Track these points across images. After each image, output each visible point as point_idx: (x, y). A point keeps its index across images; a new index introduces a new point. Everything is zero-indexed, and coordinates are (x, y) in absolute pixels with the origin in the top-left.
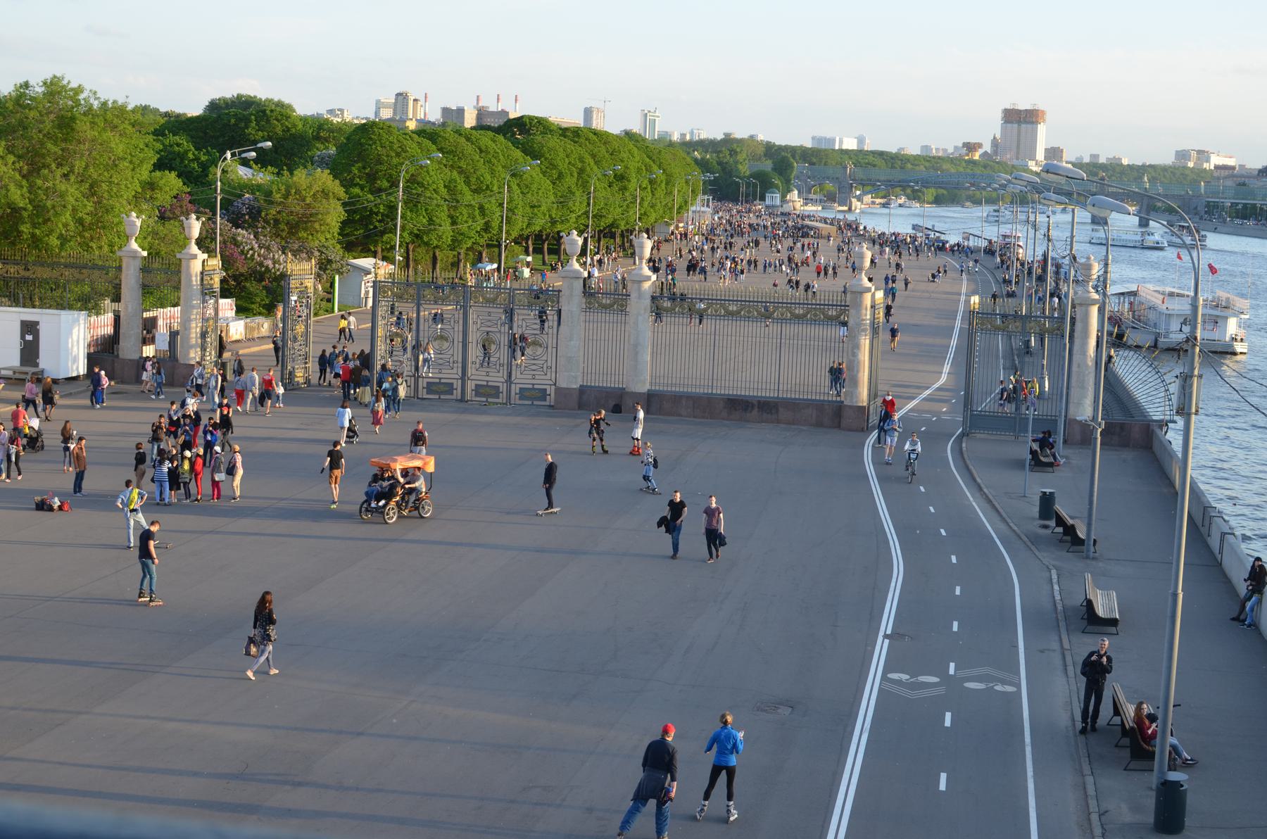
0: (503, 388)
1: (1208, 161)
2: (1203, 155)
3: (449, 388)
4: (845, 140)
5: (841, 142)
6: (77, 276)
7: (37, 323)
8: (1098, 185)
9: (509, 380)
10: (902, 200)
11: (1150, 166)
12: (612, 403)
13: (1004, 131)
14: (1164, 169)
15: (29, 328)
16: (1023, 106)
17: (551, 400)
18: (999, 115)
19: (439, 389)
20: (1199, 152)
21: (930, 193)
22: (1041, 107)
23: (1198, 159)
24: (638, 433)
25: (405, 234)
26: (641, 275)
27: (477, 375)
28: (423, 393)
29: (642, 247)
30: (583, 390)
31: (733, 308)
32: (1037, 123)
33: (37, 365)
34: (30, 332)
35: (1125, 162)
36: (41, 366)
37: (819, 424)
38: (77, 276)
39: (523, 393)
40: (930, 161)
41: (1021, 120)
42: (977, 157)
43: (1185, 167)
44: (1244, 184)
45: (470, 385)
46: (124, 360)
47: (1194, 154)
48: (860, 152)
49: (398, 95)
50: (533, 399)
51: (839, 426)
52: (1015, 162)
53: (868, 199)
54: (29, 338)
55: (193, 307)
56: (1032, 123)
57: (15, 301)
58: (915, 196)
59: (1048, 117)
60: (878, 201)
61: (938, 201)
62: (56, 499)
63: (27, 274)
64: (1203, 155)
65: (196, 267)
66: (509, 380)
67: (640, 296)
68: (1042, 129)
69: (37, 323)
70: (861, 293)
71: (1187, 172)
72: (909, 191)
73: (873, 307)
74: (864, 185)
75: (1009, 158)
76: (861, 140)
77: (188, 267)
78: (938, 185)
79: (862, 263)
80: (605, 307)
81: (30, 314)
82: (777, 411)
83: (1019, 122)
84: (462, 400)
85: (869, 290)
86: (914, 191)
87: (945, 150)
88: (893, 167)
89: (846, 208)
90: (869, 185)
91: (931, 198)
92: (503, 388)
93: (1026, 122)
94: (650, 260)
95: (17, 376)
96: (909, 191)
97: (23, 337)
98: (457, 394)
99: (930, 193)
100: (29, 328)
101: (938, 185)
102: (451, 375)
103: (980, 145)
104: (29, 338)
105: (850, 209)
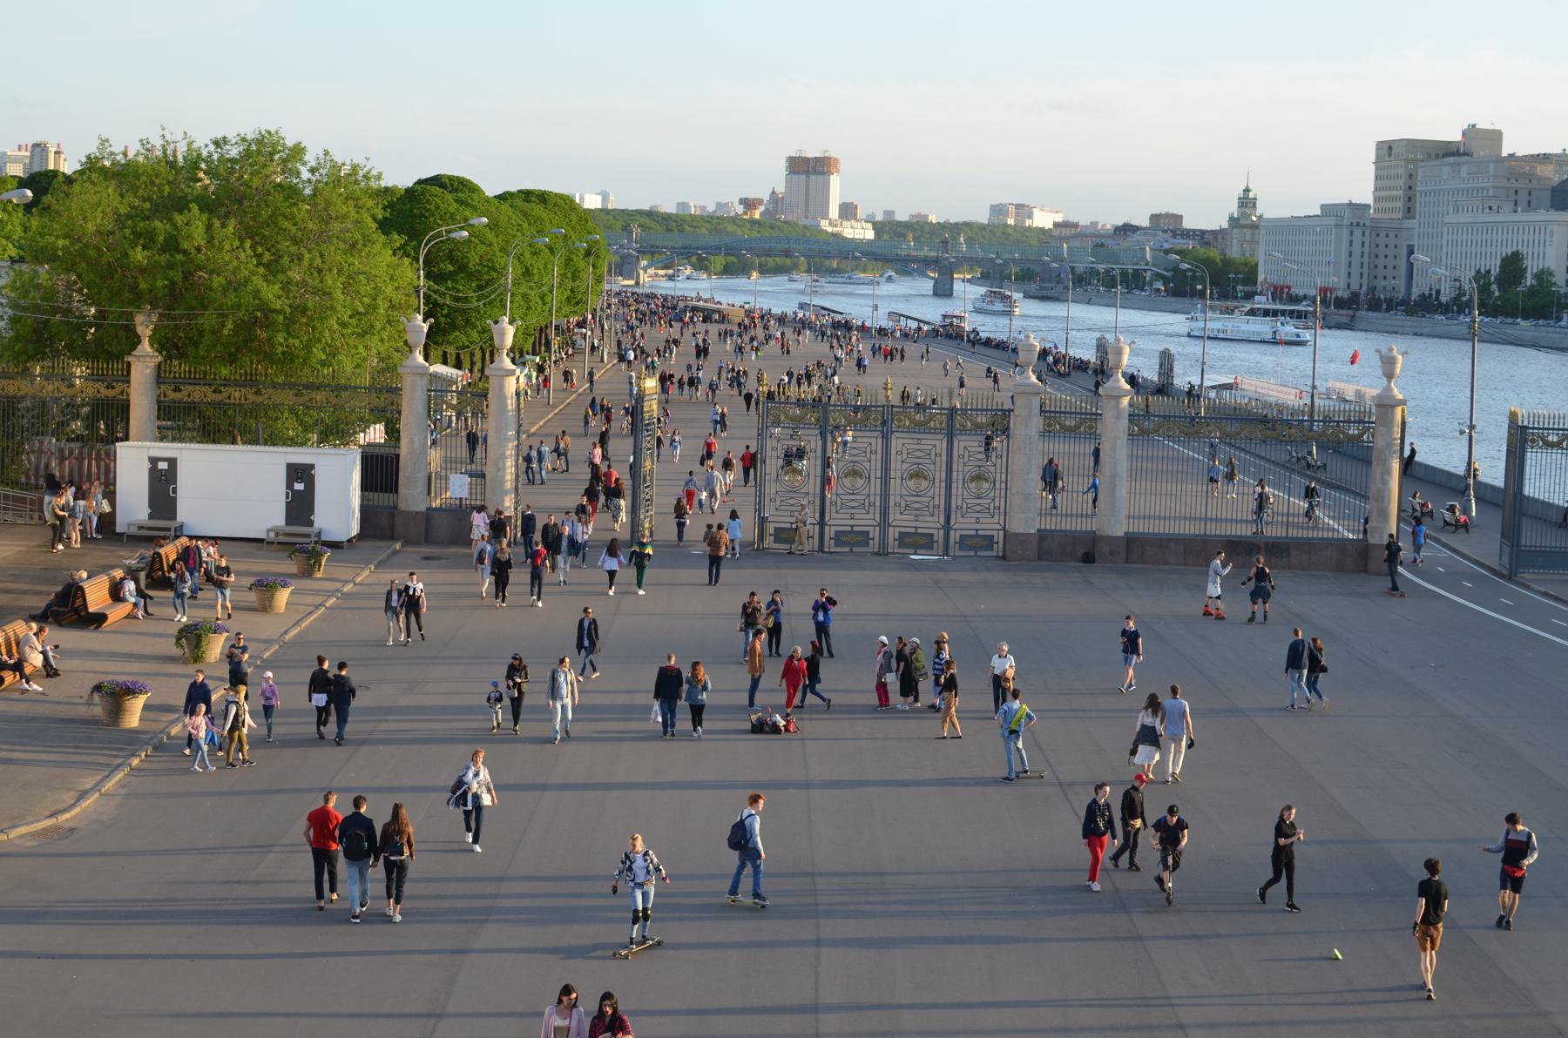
0: (875, 533)
1: (1030, 216)
2: (1024, 210)
3: (864, 537)
4: (587, 197)
5: (582, 198)
6: (334, 400)
7: (312, 466)
8: (910, 248)
9: (947, 527)
10: (688, 271)
11: (966, 224)
12: (1080, 551)
13: (788, 183)
14: (982, 227)
15: (300, 473)
16: (812, 152)
17: (998, 549)
18: (783, 164)
19: (852, 540)
20: (1018, 206)
21: (719, 261)
22: (833, 155)
23: (1017, 214)
24: (1215, 589)
25: (808, 347)
26: (502, 369)
27: (901, 521)
28: (769, 542)
29: (503, 333)
30: (1042, 535)
31: (1553, 438)
32: (829, 173)
33: (311, 524)
34: (300, 479)
35: (933, 219)
36: (317, 524)
37: (1340, 569)
38: (334, 400)
39: (964, 542)
40: (715, 221)
41: (810, 170)
42: (757, 216)
43: (1006, 225)
44: (1102, 245)
45: (893, 533)
46: (409, 513)
47: (1012, 209)
48: (604, 211)
49: (36, 146)
50: (975, 548)
51: (1365, 570)
52: (804, 221)
53: (651, 271)
54: (299, 486)
55: (508, 440)
56: (823, 173)
57: (273, 440)
58: (701, 265)
59: (842, 166)
60: (661, 272)
61: (728, 271)
62: (778, 717)
63: (259, 399)
64: (1024, 210)
65: (511, 385)
66: (947, 527)
67: (1118, 416)
68: (835, 181)
69: (312, 466)
70: (1393, 407)
71: (1009, 231)
72: (694, 259)
73: (518, 394)
74: (653, 254)
75: (794, 215)
76: (605, 198)
77: (502, 387)
78: (729, 251)
79: (503, 340)
80: (1069, 430)
81: (300, 456)
82: (1289, 555)
83: (807, 173)
84: (882, 553)
85: (512, 373)
86: (700, 259)
87: (703, 208)
88: (669, 230)
89: (632, 282)
90: (649, 250)
91: (719, 268)
92: (875, 533)
93: (816, 173)
94: (512, 350)
95: (281, 539)
96: (694, 259)
97: (289, 485)
98: (875, 544)
99: (719, 261)
100: (300, 473)
101: (729, 251)
102: (866, 521)
103: (760, 202)
104: (299, 486)
105: (637, 283)
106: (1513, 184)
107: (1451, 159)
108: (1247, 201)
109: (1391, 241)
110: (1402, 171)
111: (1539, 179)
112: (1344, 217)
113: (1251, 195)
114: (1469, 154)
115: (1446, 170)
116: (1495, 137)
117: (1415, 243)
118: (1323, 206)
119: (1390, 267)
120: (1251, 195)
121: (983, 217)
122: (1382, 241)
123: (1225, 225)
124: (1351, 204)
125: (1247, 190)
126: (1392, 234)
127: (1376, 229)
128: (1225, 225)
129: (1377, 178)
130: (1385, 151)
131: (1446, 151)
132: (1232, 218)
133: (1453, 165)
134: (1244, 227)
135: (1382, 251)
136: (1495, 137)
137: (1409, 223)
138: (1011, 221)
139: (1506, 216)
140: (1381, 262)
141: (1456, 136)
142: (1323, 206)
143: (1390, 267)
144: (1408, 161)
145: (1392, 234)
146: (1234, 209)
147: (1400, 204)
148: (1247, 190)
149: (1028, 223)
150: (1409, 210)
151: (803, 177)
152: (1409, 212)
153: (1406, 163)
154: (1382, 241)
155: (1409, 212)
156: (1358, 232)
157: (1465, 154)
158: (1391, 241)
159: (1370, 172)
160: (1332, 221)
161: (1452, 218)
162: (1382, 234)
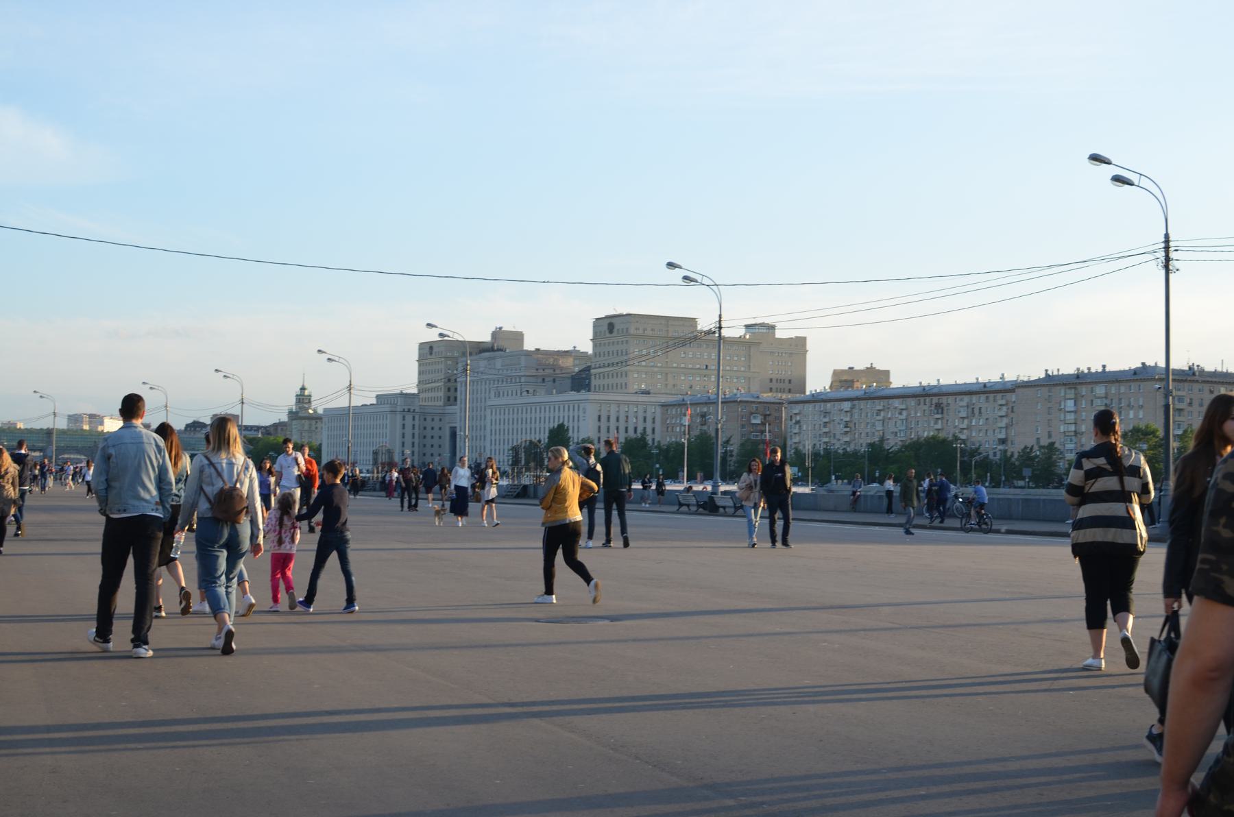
1: (102, 423)
7: (804, 339)
20: (92, 416)
35: (20, 425)
47: (86, 419)
69: (804, 339)
106: (541, 373)
107: (487, 354)
108: (303, 398)
109: (436, 424)
110: (442, 366)
111: (562, 368)
112: (393, 405)
113: (307, 393)
114: (500, 349)
115: (483, 363)
116: (518, 337)
117: (457, 425)
118: (378, 397)
119: (436, 446)
120: (307, 393)
121: (62, 424)
122: (429, 424)
123: (285, 418)
124: (402, 394)
125: (303, 389)
126: (437, 419)
127: (424, 415)
128: (285, 418)
129: (420, 373)
130: (427, 350)
131: (479, 349)
132: (291, 413)
133: (489, 359)
134: (305, 418)
135: (429, 433)
136: (518, 337)
137: (450, 409)
138: (86, 427)
139: (541, 398)
140: (428, 441)
141: (486, 337)
142: (378, 397)
143: (436, 446)
144: (447, 358)
145: (437, 419)
146: (291, 402)
147: (441, 394)
148: (303, 389)
149: (100, 428)
150: (449, 398)
151: (1174, 365)
152: (451, 399)
153: (446, 361)
154: (429, 424)
155: (451, 399)
156: (409, 417)
157: (499, 350)
158: (436, 424)
159: (414, 368)
160: (387, 408)
161: (494, 401)
162: (429, 418)
